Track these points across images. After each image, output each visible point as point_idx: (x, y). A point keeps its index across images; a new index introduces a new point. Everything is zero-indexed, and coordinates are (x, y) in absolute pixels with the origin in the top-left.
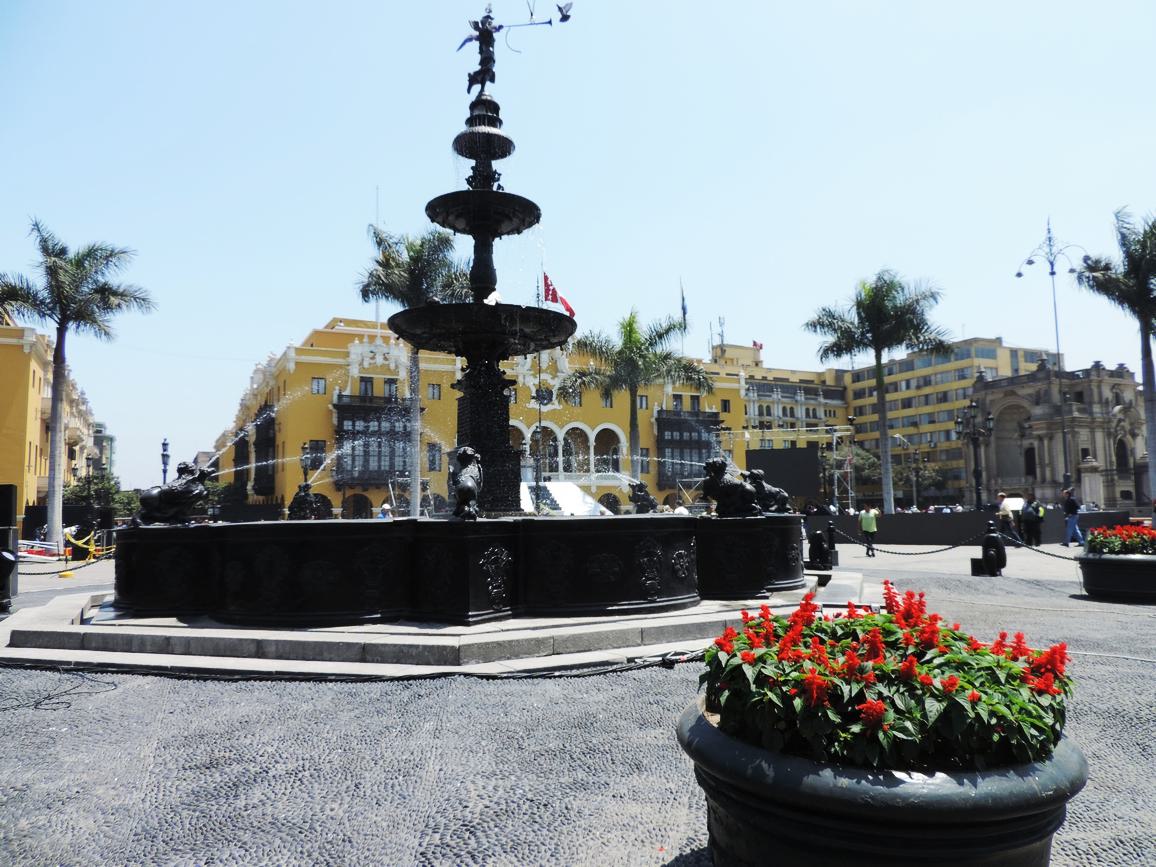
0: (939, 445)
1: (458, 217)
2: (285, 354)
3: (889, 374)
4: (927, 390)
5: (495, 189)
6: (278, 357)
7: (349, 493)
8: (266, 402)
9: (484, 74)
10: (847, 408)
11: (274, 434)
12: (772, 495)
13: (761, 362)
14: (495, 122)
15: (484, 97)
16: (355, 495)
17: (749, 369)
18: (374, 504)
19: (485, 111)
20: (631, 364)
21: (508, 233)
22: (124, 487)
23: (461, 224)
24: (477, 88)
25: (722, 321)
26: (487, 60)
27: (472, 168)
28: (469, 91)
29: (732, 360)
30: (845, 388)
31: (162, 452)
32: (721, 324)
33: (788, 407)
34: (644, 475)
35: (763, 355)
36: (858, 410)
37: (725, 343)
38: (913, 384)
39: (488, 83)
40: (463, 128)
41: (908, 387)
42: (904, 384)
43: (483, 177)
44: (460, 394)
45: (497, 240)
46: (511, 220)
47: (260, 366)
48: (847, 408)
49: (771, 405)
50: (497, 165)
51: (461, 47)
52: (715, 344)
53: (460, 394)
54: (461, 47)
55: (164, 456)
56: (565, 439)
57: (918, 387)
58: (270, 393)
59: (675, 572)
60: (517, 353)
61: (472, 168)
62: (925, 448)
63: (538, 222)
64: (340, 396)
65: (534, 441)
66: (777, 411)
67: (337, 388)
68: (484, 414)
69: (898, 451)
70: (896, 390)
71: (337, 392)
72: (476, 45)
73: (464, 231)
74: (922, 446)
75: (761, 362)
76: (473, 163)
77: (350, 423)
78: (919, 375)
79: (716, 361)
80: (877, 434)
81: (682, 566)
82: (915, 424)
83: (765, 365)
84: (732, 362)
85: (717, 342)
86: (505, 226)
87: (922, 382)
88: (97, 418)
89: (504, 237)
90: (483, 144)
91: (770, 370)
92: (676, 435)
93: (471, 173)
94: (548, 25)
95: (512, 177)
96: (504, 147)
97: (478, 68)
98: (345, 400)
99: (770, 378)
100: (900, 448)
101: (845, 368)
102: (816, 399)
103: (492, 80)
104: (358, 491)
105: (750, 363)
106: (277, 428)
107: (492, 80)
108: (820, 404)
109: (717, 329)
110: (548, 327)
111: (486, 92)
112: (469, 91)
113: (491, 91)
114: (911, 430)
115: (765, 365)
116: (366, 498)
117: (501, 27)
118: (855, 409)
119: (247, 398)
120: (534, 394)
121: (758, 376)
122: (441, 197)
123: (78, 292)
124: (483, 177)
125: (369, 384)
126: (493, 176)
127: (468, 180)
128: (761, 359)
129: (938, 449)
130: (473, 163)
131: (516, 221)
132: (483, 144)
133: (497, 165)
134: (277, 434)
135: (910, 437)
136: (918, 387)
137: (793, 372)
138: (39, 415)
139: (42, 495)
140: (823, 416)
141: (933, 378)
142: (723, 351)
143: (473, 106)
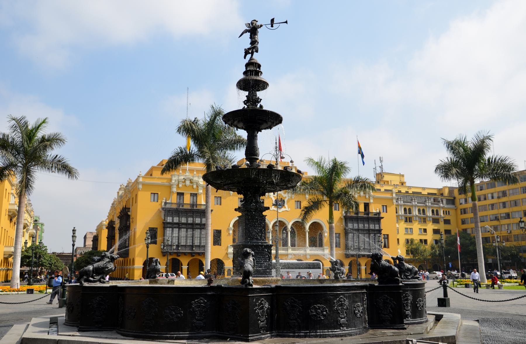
0: (512, 232)
1: (239, 122)
2: (137, 179)
3: (481, 190)
4: (504, 199)
5: (258, 106)
6: (133, 181)
7: (170, 257)
8: (126, 206)
9: (253, 49)
10: (456, 209)
11: (130, 224)
12: (409, 270)
13: (405, 183)
14: (257, 73)
15: (253, 61)
16: (173, 259)
17: (398, 187)
18: (183, 264)
19: (253, 68)
20: (329, 184)
21: (265, 129)
22: (49, 251)
23: (241, 125)
24: (249, 56)
25: (381, 159)
26: (254, 42)
27: (246, 96)
28: (245, 58)
29: (388, 182)
30: (455, 198)
31: (72, 235)
32: (381, 161)
33: (421, 209)
34: (337, 248)
35: (405, 179)
36: (463, 211)
37: (385, 170)
38: (495, 195)
39: (255, 53)
40: (242, 76)
41: (493, 198)
42: (490, 196)
43: (252, 100)
44: (240, 214)
45: (259, 132)
46: (267, 122)
47: (122, 186)
48: (456, 209)
49: (411, 208)
50: (260, 94)
51: (240, 36)
52: (377, 172)
53: (240, 214)
54: (240, 36)
55: (73, 236)
56: (291, 228)
57: (499, 198)
58: (128, 201)
59: (356, 314)
60: (270, 191)
61: (246, 96)
62: (504, 233)
63: (281, 123)
64: (166, 203)
65: (274, 225)
66: (415, 212)
67: (164, 198)
68: (252, 217)
69: (487, 235)
70: (485, 199)
71: (164, 201)
72: (248, 34)
73: (242, 128)
74: (502, 232)
75: (405, 183)
76: (247, 93)
77: (171, 218)
78: (498, 190)
79: (378, 182)
80: (473, 225)
81: (359, 311)
82: (497, 219)
83: (407, 184)
84: (388, 183)
85: (379, 171)
86: (263, 126)
87: (501, 195)
88: (35, 214)
89: (263, 131)
90: (252, 82)
91: (410, 187)
92: (356, 225)
93: (246, 99)
94: (286, 24)
95: (268, 100)
96: (264, 85)
97: (249, 46)
98: (168, 206)
99: (410, 191)
100: (489, 233)
101: (454, 186)
102: (438, 204)
103: (257, 51)
104: (174, 256)
105: (398, 183)
106: (131, 220)
107: (257, 51)
108: (440, 207)
109: (379, 164)
110: (287, 179)
111: (254, 57)
112: (245, 58)
113: (257, 57)
114: (495, 223)
115: (407, 184)
116: (179, 260)
117: (261, 26)
118: (461, 210)
119: (116, 203)
120: (274, 203)
121: (403, 190)
122: (231, 112)
123: (29, 151)
124: (252, 100)
125: (156, 195)
126: (258, 100)
127: (244, 102)
128: (405, 181)
129: (513, 234)
130: (247, 93)
131: (269, 123)
132: (252, 82)
133: (260, 94)
134: (131, 224)
135: (496, 228)
136: (499, 198)
137: (424, 189)
138: (7, 213)
139: (6, 256)
140: (442, 214)
141: (507, 192)
142: (382, 177)
143: (247, 65)
